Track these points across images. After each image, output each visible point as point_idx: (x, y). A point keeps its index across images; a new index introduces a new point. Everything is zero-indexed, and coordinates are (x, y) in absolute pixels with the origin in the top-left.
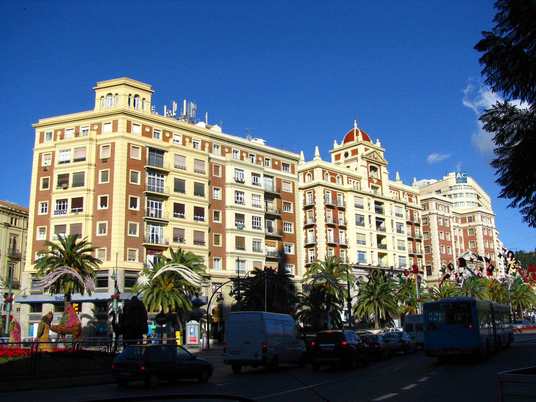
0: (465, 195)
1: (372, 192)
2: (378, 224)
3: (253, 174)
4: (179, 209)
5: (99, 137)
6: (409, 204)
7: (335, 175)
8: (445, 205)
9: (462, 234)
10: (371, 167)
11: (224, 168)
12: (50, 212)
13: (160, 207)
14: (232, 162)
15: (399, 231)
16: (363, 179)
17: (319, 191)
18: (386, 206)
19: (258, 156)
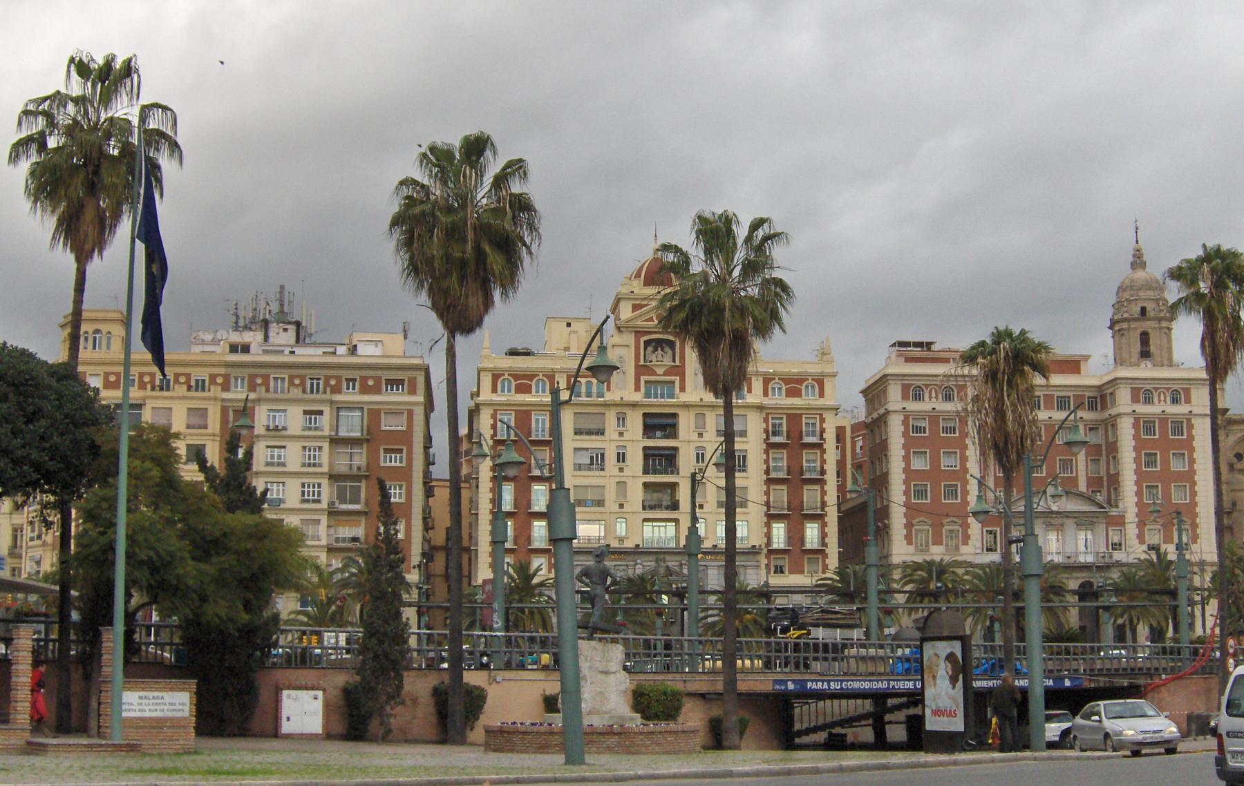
13: (303, 492)
18: (686, 423)
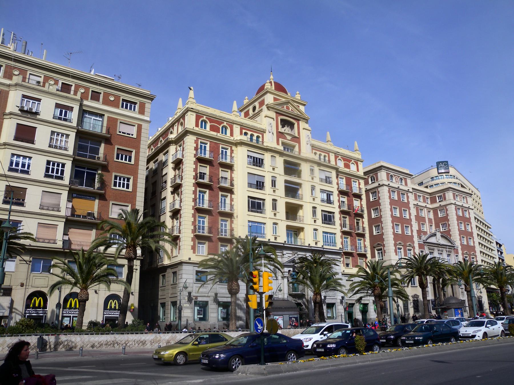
3: (57, 106)
8: (401, 177)
9: (431, 216)
10: (282, 120)
14: (16, 85)
15: (329, 201)
16: (267, 132)
18: (305, 168)
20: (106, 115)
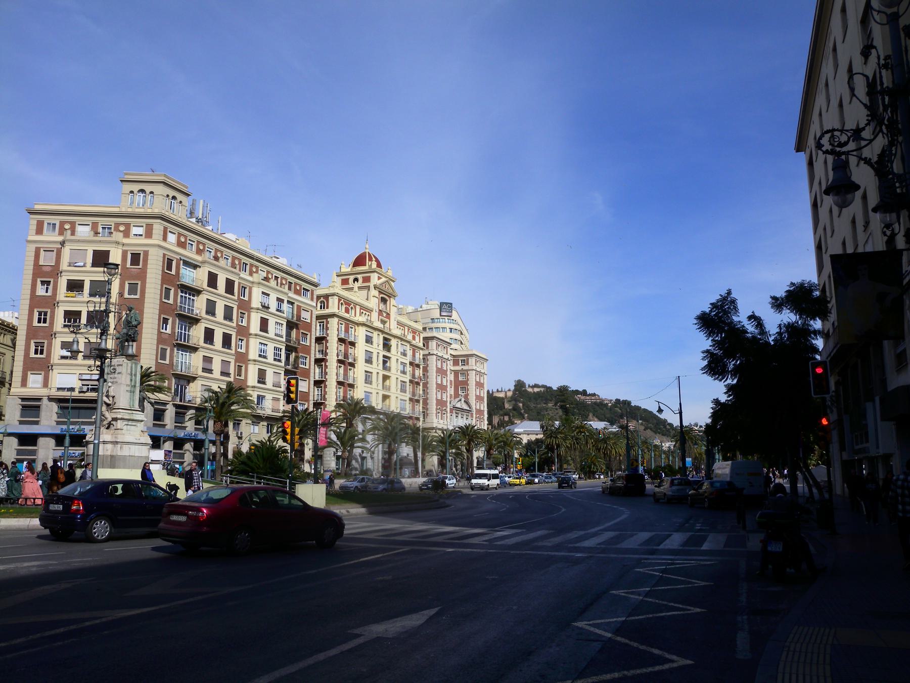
0: (448, 330)
1: (382, 326)
2: (385, 362)
4: (209, 335)
5: (126, 241)
6: (414, 342)
7: (349, 305)
11: (250, 289)
12: (52, 323)
15: (404, 372)
17: (333, 322)
18: (394, 342)
19: (282, 278)
20: (296, 303)
